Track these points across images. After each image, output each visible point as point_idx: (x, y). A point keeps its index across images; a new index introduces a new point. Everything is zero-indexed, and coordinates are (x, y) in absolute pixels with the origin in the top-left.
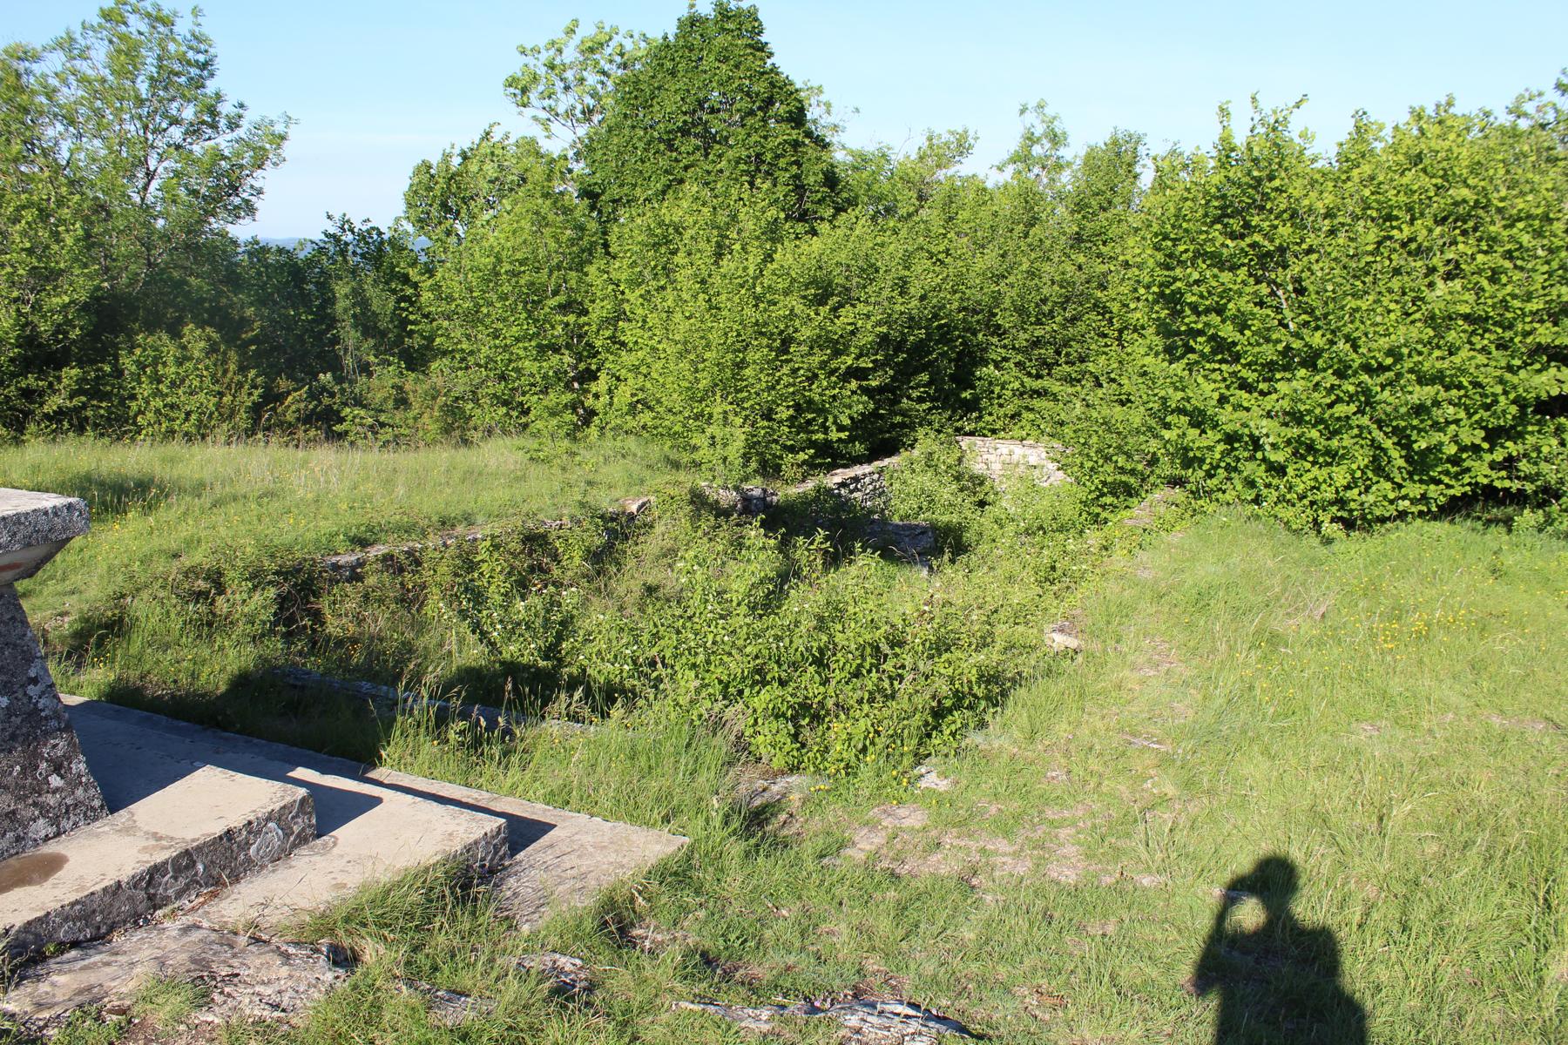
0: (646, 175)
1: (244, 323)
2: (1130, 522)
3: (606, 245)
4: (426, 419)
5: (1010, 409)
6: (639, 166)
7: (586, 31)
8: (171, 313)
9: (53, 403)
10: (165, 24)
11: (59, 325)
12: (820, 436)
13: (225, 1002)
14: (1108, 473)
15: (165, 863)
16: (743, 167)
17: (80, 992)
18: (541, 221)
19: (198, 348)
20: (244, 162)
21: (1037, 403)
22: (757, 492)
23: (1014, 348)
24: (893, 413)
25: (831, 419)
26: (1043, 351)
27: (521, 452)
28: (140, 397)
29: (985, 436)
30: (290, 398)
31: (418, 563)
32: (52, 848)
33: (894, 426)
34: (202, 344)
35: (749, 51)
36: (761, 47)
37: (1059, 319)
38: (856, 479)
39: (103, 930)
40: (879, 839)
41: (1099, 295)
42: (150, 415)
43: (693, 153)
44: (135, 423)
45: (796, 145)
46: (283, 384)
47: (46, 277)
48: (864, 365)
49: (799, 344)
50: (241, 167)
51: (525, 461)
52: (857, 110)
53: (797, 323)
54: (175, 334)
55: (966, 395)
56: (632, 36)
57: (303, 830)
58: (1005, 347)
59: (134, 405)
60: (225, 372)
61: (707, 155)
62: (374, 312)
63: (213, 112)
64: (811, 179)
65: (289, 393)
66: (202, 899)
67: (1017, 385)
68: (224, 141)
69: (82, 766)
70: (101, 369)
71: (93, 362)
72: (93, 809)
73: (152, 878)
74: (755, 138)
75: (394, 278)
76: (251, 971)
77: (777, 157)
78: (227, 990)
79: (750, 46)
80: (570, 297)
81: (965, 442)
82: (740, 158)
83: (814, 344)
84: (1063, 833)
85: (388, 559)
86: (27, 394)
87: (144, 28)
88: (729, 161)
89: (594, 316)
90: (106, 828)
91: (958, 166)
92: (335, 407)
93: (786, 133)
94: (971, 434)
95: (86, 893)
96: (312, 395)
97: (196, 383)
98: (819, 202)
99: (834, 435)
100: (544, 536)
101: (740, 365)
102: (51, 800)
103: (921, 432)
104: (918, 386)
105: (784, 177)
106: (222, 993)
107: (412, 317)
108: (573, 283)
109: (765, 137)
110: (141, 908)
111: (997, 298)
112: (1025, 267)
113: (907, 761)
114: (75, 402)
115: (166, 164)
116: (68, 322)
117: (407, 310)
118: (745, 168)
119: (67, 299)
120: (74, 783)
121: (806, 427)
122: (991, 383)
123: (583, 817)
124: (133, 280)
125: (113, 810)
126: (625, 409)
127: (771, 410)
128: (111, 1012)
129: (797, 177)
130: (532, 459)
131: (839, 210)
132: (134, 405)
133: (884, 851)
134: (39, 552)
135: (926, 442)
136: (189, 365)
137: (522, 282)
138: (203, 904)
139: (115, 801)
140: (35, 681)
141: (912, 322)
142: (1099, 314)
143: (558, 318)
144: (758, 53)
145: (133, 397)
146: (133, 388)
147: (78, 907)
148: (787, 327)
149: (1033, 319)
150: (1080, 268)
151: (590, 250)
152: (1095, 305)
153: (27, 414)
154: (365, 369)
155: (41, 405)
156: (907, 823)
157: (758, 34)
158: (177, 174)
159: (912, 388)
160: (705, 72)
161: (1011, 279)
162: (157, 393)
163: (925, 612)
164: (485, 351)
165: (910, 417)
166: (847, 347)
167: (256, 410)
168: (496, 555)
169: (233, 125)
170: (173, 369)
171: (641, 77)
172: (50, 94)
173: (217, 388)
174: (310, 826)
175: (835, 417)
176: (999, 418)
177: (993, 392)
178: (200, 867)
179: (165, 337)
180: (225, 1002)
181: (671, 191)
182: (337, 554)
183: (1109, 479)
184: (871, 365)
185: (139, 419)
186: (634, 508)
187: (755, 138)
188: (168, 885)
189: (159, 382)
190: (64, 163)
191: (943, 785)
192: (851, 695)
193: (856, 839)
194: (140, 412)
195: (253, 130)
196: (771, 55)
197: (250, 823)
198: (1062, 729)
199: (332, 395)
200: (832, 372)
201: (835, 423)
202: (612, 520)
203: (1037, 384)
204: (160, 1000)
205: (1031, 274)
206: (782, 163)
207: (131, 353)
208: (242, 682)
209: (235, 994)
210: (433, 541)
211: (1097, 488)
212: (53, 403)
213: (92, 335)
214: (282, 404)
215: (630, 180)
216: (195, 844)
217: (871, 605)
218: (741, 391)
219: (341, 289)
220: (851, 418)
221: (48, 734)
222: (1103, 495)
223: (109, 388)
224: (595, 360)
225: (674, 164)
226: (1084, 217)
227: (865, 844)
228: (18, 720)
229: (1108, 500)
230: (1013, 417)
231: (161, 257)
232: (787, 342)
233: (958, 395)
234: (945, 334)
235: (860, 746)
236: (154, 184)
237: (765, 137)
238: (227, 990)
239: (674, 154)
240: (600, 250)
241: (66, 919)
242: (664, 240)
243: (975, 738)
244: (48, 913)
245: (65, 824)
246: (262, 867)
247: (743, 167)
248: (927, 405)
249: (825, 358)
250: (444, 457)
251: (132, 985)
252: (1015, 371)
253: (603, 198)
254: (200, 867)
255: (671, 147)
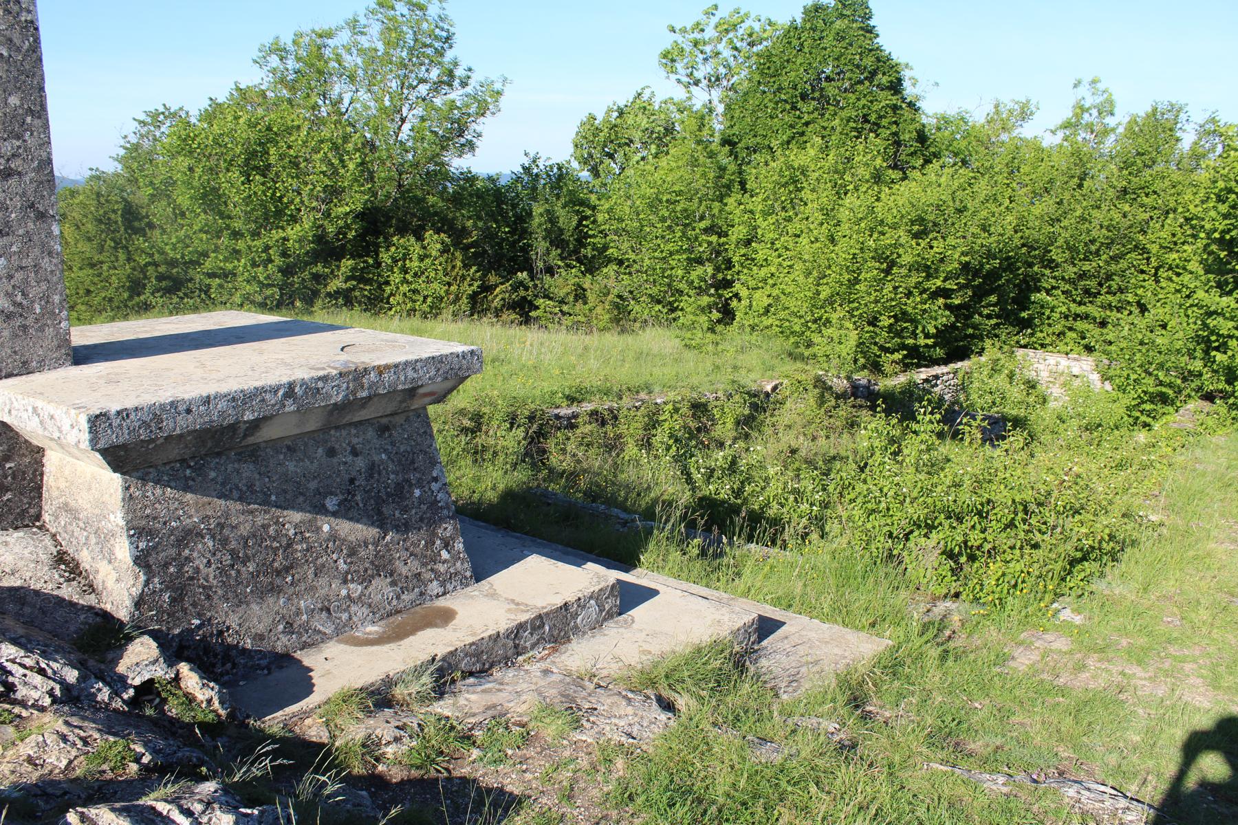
0: (775, 129)
1: (464, 232)
2: (1175, 426)
3: (743, 184)
4: (599, 310)
5: (1058, 328)
6: (769, 121)
7: (723, 13)
8: (415, 222)
9: (335, 285)
10: (421, 9)
11: (341, 228)
12: (910, 341)
13: (592, 728)
14: (1149, 385)
15: (526, 622)
16: (852, 124)
17: (488, 708)
18: (694, 163)
19: (435, 249)
20: (471, 111)
21: (1080, 325)
22: (864, 382)
23: (1063, 279)
24: (966, 326)
25: (920, 328)
26: (1088, 283)
27: (678, 340)
28: (392, 283)
29: (1035, 348)
30: (498, 289)
31: (616, 418)
32: (442, 603)
33: (967, 336)
34: (439, 246)
35: (861, 32)
36: (869, 30)
37: (1104, 257)
38: (937, 377)
39: (487, 666)
40: (1035, 656)
41: (1141, 238)
42: (399, 298)
43: (812, 113)
44: (388, 303)
45: (895, 108)
46: (493, 279)
47: (334, 193)
48: (949, 287)
49: (901, 266)
50: (469, 115)
51: (681, 347)
52: (937, 84)
53: (901, 251)
54: (420, 238)
55: (1024, 315)
56: (759, 20)
57: (611, 608)
58: (1054, 278)
59: (388, 289)
60: (454, 267)
61: (823, 115)
62: (559, 228)
63: (451, 74)
64: (907, 137)
65: (496, 286)
66: (547, 652)
67: (1064, 309)
68: (456, 95)
69: (461, 546)
70: (365, 262)
71: (361, 256)
72: (466, 578)
73: (518, 632)
74: (863, 101)
75: (577, 203)
76: (605, 707)
77: (880, 117)
78: (592, 719)
79: (862, 28)
80: (713, 221)
81: (1020, 353)
82: (850, 117)
83: (913, 268)
84: (1188, 667)
85: (594, 413)
86: (317, 277)
87: (405, 12)
88: (842, 120)
89: (733, 238)
90: (476, 593)
91: (1019, 130)
92: (529, 298)
93: (886, 98)
94: (1025, 347)
95: (479, 638)
96: (515, 288)
97: (433, 274)
98: (912, 154)
99: (922, 341)
100: (705, 405)
101: (857, 281)
102: (442, 568)
103: (988, 343)
104: (989, 305)
105: (885, 133)
106: (588, 720)
107: (590, 233)
108: (716, 211)
109: (872, 102)
110: (510, 653)
111: (1052, 239)
112: (1078, 213)
113: (1048, 597)
114: (348, 285)
115: (415, 112)
116: (348, 226)
117: (587, 226)
118: (854, 125)
119: (348, 209)
120: (456, 558)
121: (899, 334)
122: (1042, 307)
123: (805, 619)
124: (388, 196)
125: (478, 580)
126: (762, 311)
127: (876, 319)
128: (514, 724)
129: (895, 134)
130: (686, 345)
131: (927, 161)
132: (388, 289)
133: (1040, 666)
134: (449, 384)
135: (991, 352)
136: (427, 261)
137: (678, 208)
138: (549, 655)
139: (479, 575)
140: (436, 479)
141: (990, 255)
142: (1139, 254)
143: (704, 237)
144: (868, 35)
145: (387, 283)
146: (388, 276)
147: (474, 647)
148: (892, 253)
149: (1082, 256)
150: (1125, 216)
151: (728, 187)
152: (1136, 246)
153: (316, 293)
154: (550, 270)
155: (325, 286)
156: (1055, 646)
157: (868, 19)
158: (423, 119)
159: (983, 307)
160: (825, 49)
161: (1065, 223)
162: (405, 281)
163: (1064, 481)
164: (647, 262)
165: (979, 329)
166: (937, 270)
167: (473, 297)
168: (676, 416)
169: (464, 84)
170: (417, 264)
171: (774, 52)
172: (339, 60)
173: (447, 279)
174: (615, 606)
175: (924, 327)
176: (1048, 335)
177: (1044, 314)
178: (547, 628)
179: (412, 239)
180: (592, 728)
181: (794, 142)
182: (557, 407)
183: (1151, 390)
184: (955, 287)
185: (391, 299)
186: (769, 388)
187: (863, 101)
188: (527, 639)
189: (406, 273)
190: (344, 110)
191: (1078, 620)
192: (1004, 541)
193: (1016, 655)
194: (392, 294)
195: (478, 88)
196: (877, 36)
197: (579, 599)
198: (1169, 586)
199: (527, 289)
200: (925, 291)
201: (923, 331)
202: (755, 396)
203: (1081, 310)
204: (548, 720)
205: (1083, 219)
206: (884, 122)
207: (388, 250)
208: (509, 496)
209: (598, 723)
210: (626, 401)
211: (1139, 396)
212: (335, 285)
213: (361, 236)
214: (492, 293)
215: (761, 132)
216: (545, 611)
217: (1019, 472)
218: (853, 302)
219: (538, 209)
220: (936, 328)
221: (442, 520)
222: (1143, 402)
223: (371, 276)
224: (730, 272)
225: (797, 120)
226: (1130, 174)
227: (1023, 661)
228: (425, 507)
229: (1148, 407)
230: (1058, 335)
231: (407, 180)
232: (892, 264)
233: (1016, 314)
234: (1009, 264)
235: (1013, 582)
236: (406, 127)
237: (872, 102)
238: (592, 719)
239: (798, 113)
240: (737, 186)
241: (466, 655)
242: (794, 181)
243: (1098, 586)
244: (457, 649)
245: (449, 587)
246: (584, 633)
247: (852, 124)
248: (993, 321)
249: (920, 279)
250: (612, 339)
251: (525, 707)
252: (1062, 298)
253: (740, 145)
254: (547, 628)
255: (794, 108)
